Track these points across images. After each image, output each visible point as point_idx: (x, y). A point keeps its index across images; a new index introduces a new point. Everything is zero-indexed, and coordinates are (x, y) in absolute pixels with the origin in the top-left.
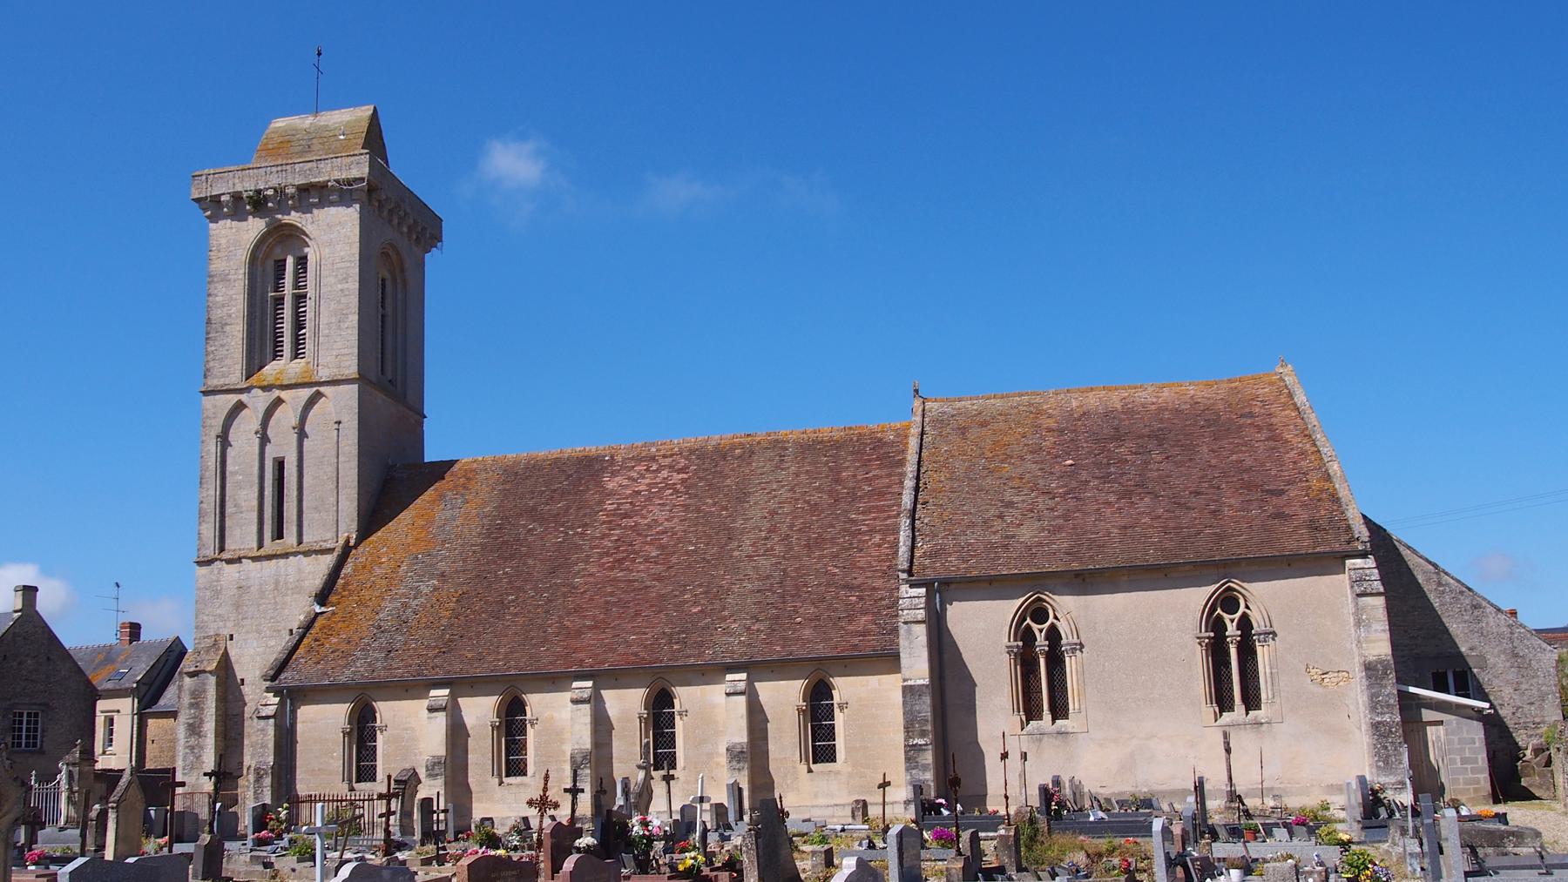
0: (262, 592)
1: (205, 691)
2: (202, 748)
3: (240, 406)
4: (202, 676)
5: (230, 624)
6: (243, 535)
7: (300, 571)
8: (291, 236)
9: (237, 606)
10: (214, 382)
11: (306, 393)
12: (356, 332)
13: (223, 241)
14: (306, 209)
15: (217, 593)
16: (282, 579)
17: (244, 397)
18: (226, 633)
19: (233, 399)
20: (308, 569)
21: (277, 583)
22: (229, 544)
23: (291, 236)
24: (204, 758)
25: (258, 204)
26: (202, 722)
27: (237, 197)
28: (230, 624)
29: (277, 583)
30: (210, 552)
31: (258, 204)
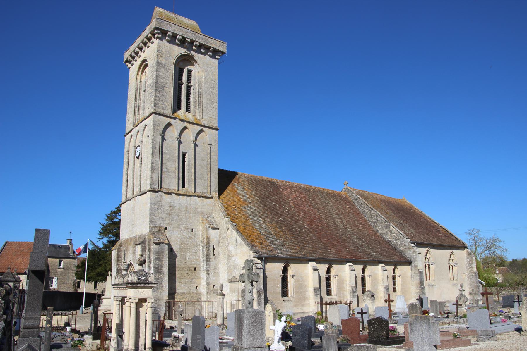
0: (180, 210)
1: (163, 253)
2: (162, 279)
3: (169, 124)
4: (162, 245)
5: (166, 222)
6: (171, 182)
7: (196, 204)
8: (188, 60)
9: (169, 214)
10: (159, 110)
11: (199, 128)
12: (217, 110)
13: (164, 51)
14: (198, 51)
15: (160, 207)
16: (189, 206)
17: (172, 121)
18: (164, 226)
19: (168, 120)
20: (199, 204)
21: (186, 207)
22: (164, 186)
23: (188, 60)
24: (163, 284)
25: (183, 42)
26: (162, 267)
27: (174, 36)
28: (166, 222)
29: (186, 207)
30: (157, 187)
31: (183, 42)
